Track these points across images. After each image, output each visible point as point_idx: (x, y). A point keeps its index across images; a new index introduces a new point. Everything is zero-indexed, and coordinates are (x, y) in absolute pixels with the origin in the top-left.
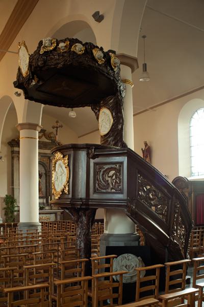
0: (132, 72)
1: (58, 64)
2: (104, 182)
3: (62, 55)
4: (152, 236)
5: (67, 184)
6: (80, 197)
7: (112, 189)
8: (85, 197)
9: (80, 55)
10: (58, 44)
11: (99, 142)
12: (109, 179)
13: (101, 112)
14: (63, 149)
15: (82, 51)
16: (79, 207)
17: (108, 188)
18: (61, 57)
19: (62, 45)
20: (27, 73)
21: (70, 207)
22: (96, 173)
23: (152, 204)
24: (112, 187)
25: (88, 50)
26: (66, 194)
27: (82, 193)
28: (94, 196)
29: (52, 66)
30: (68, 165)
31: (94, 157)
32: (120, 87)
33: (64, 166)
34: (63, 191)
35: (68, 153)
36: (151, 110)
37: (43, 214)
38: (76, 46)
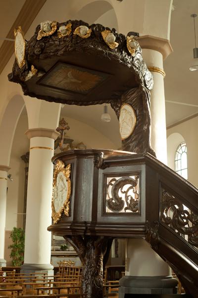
1: (57, 50)
3: (63, 39)
4: (188, 279)
5: (67, 203)
6: (83, 220)
7: (126, 209)
8: (91, 220)
10: (58, 28)
18: (62, 43)
19: (62, 28)
20: (22, 64)
29: (51, 54)
30: (70, 177)
34: (63, 213)
35: (71, 161)
37: (65, 256)
38: (80, 28)
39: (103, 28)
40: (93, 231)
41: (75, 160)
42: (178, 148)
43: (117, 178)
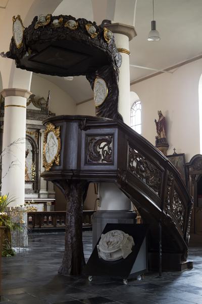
0: (129, 41)
2: (95, 153)
6: (71, 168)
9: (73, 30)
11: (93, 113)
12: (101, 150)
13: (96, 82)
14: (55, 120)
15: (75, 26)
16: (70, 178)
17: (99, 160)
19: (56, 22)
20: (21, 46)
21: (61, 178)
22: (87, 145)
23: (143, 176)
24: (103, 158)
25: (81, 26)
26: (57, 165)
27: (73, 165)
28: (84, 167)
30: (60, 136)
31: (86, 128)
32: (115, 57)
33: (55, 138)
34: (54, 163)
35: (61, 124)
36: (166, 72)
39: (87, 21)
40: (79, 176)
41: (65, 124)
42: (133, 106)
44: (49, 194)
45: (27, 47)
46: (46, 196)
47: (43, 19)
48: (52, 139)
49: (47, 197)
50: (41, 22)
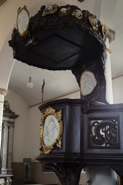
26: (58, 148)
27: (77, 148)
30: (61, 119)
31: (88, 113)
34: (55, 146)
39: (90, 14)
43: (99, 121)
44: (8, 171)
45: (32, 34)
46: (6, 173)
47: (50, 8)
48: (52, 122)
49: (6, 173)
50: (48, 11)
